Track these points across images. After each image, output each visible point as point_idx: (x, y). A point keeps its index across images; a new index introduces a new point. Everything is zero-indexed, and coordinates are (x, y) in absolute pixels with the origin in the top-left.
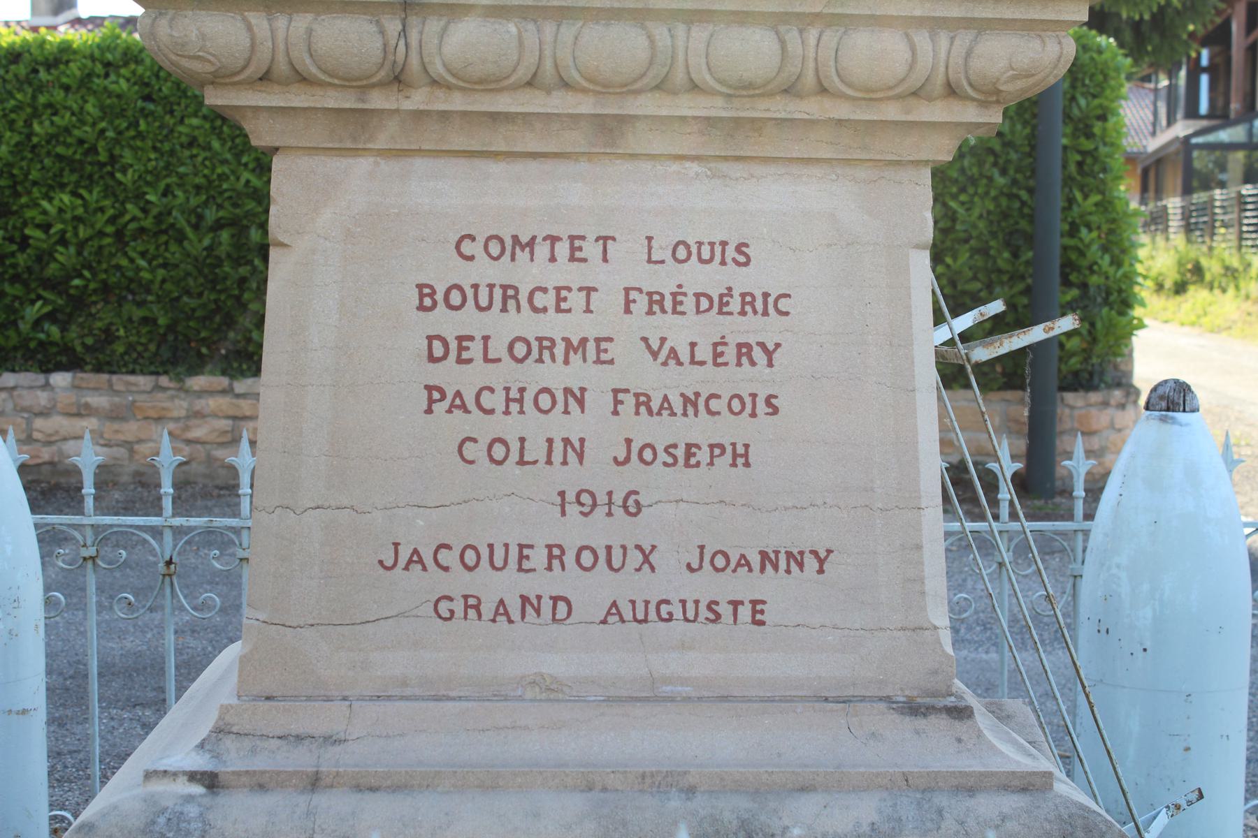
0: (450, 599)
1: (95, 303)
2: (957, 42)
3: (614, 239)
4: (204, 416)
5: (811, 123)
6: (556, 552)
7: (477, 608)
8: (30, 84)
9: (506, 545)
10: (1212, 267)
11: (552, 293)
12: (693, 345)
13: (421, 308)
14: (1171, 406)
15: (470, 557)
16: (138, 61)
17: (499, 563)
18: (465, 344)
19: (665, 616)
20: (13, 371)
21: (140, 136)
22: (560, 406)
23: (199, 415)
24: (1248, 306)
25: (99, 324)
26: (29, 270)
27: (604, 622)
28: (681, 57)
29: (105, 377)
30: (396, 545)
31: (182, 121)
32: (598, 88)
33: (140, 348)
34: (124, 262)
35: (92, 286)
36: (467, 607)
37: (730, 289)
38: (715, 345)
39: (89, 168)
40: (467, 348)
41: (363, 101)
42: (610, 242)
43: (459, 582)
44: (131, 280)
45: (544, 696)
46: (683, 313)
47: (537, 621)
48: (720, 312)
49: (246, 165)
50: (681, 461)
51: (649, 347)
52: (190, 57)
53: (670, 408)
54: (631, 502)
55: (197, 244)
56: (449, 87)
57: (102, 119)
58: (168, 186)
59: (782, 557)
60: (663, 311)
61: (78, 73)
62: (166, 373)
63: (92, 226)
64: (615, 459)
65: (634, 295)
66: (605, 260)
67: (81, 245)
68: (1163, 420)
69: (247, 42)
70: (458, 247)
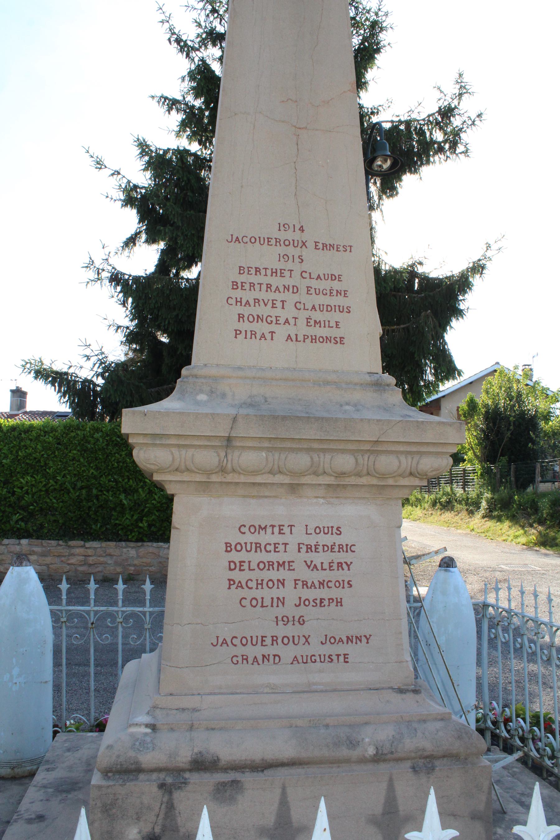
0: (237, 656)
1: (38, 515)
2: (414, 459)
3: (294, 526)
4: (75, 555)
5: (363, 486)
6: (275, 638)
7: (247, 659)
8: (19, 438)
9: (257, 637)
10: (412, 498)
11: (273, 546)
12: (322, 563)
13: (226, 551)
14: (448, 566)
15: (244, 641)
16: (56, 431)
17: (254, 643)
18: (242, 564)
19: (313, 661)
20: (8, 538)
21: (55, 456)
22: (276, 586)
23: (73, 555)
24: (424, 512)
25: (39, 522)
26: (15, 503)
27: (292, 663)
28: (322, 464)
29: (40, 541)
30: (218, 637)
31: (70, 452)
32: (292, 474)
33: (52, 531)
34: (48, 500)
35: (37, 509)
36: (243, 659)
37: (334, 543)
38: (330, 563)
39: (37, 468)
40: (243, 566)
41: (209, 478)
42: (293, 527)
43: (240, 650)
44: (50, 507)
45: (270, 691)
46: (319, 552)
47: (268, 664)
48: (331, 551)
49: (92, 467)
50: (318, 605)
51: (307, 564)
52: (150, 464)
53: (315, 586)
54: (301, 620)
55: (74, 495)
56: (240, 473)
57: (43, 451)
58: (64, 474)
59: (354, 638)
60: (312, 551)
61: (35, 435)
62: (61, 540)
63: (38, 488)
64: (295, 605)
65: (301, 546)
66: (291, 533)
67: (33, 494)
68: (446, 571)
69: (171, 459)
70: (239, 529)
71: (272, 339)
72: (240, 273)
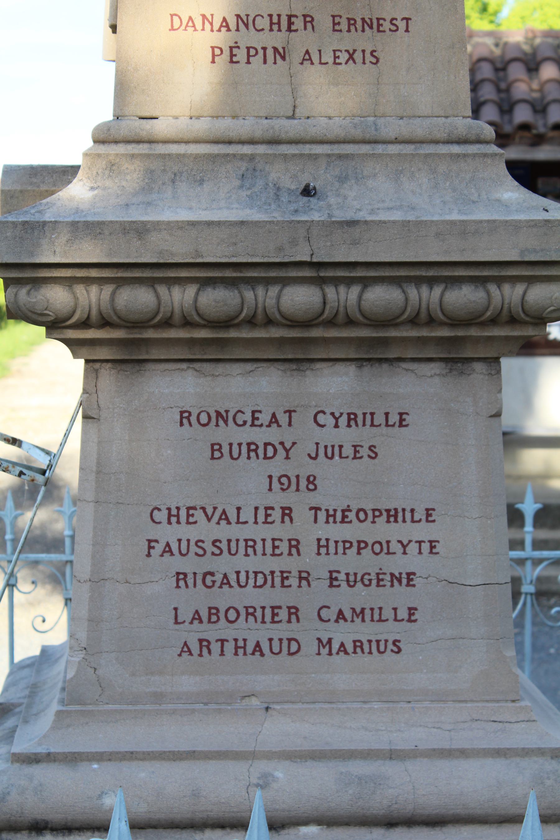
71: (290, 424)
72: (213, 458)
